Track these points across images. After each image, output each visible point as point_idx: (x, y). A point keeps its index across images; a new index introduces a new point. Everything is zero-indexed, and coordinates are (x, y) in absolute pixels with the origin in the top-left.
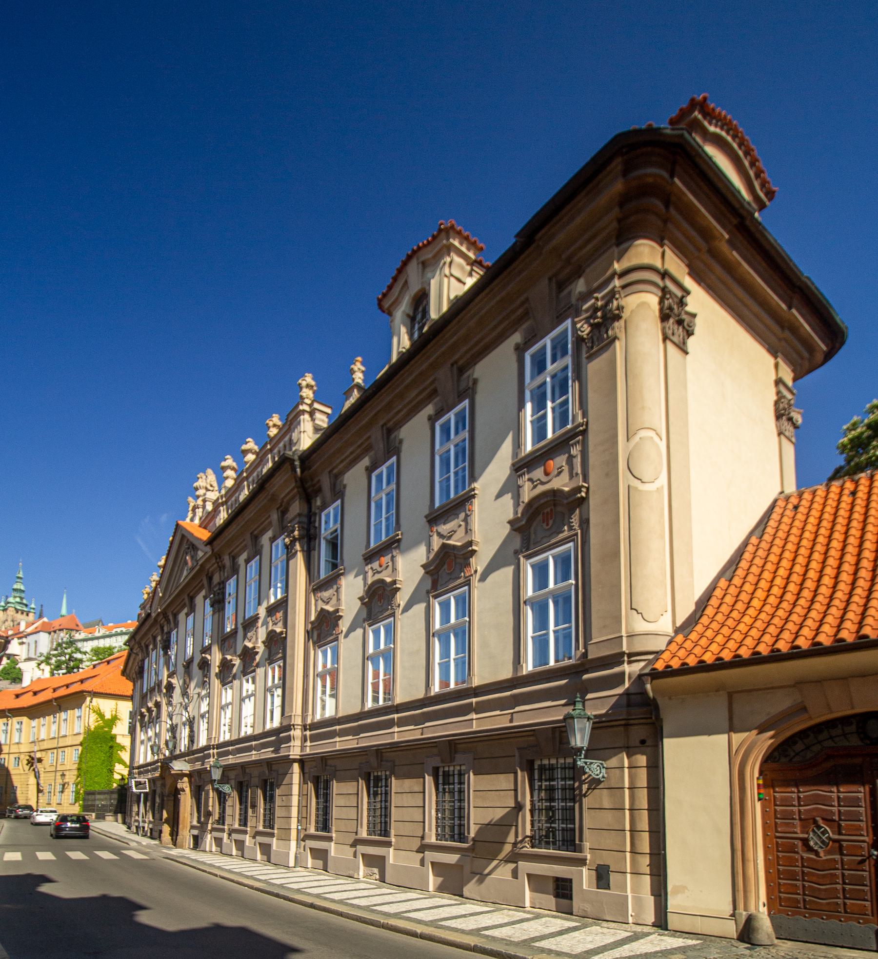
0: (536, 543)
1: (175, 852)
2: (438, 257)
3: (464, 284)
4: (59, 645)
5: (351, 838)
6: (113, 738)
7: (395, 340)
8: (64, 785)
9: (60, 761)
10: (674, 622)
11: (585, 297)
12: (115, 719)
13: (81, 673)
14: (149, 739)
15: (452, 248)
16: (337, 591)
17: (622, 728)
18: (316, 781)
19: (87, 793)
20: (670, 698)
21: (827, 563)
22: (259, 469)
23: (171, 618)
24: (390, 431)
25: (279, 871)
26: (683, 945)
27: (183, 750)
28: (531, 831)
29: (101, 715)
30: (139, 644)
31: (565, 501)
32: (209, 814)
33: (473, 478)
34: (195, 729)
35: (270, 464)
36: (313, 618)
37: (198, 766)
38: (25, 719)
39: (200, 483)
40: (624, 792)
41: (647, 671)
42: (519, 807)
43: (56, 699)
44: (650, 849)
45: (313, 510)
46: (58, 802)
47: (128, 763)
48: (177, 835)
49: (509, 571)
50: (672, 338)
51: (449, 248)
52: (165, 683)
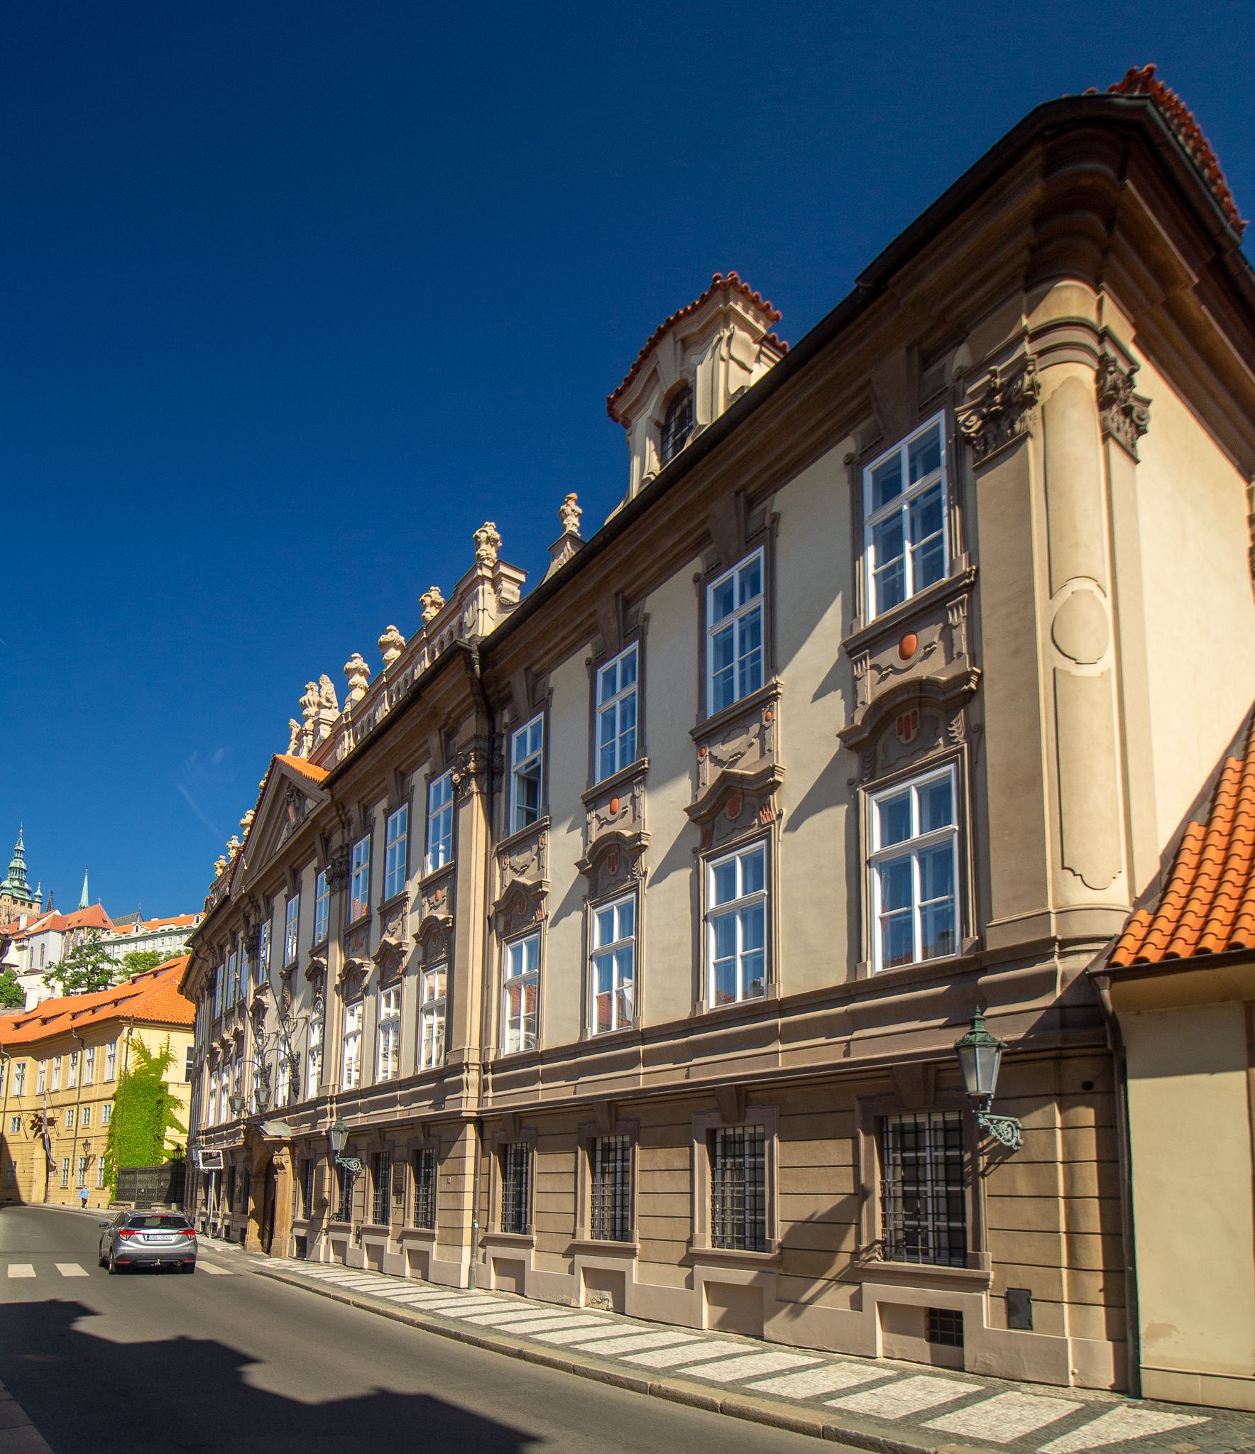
0: (887, 768)
1: (270, 1263)
2: (708, 331)
3: (750, 372)
4: (78, 950)
5: (567, 1242)
6: (163, 1087)
7: (636, 462)
8: (87, 1160)
9: (82, 1122)
10: (1132, 889)
11: (969, 375)
12: (166, 1059)
13: (110, 993)
14: (224, 1089)
15: (732, 316)
16: (538, 854)
17: (1051, 1064)
18: (503, 1152)
19: (123, 1172)
20: (1138, 1013)
21: (1235, 837)
22: (408, 671)
23: (261, 903)
24: (628, 603)
25: (446, 1294)
26: (1179, 1424)
27: (280, 1103)
28: (883, 1232)
29: (145, 1053)
30: (210, 943)
31: (941, 699)
32: (323, 1204)
33: (774, 669)
34: (301, 1072)
35: (428, 664)
36: (497, 898)
37: (305, 1129)
38: (29, 1060)
39: (311, 696)
40: (1056, 1168)
41: (1101, 967)
42: (862, 1193)
43: (76, 1029)
44: (1105, 1264)
45: (497, 730)
46: (78, 1185)
47: (186, 1126)
48: (271, 1237)
49: (838, 814)
50: (1116, 435)
51: (727, 317)
52: (251, 1002)
